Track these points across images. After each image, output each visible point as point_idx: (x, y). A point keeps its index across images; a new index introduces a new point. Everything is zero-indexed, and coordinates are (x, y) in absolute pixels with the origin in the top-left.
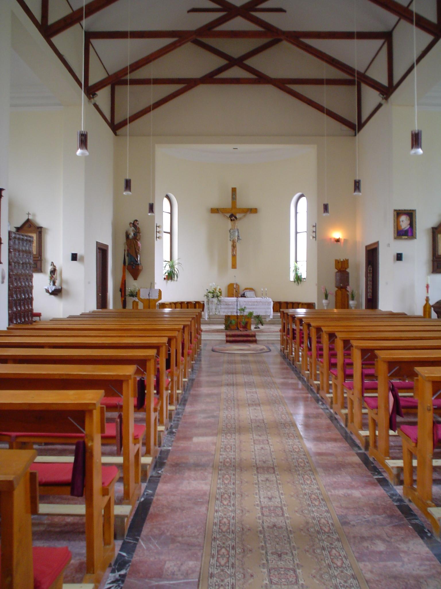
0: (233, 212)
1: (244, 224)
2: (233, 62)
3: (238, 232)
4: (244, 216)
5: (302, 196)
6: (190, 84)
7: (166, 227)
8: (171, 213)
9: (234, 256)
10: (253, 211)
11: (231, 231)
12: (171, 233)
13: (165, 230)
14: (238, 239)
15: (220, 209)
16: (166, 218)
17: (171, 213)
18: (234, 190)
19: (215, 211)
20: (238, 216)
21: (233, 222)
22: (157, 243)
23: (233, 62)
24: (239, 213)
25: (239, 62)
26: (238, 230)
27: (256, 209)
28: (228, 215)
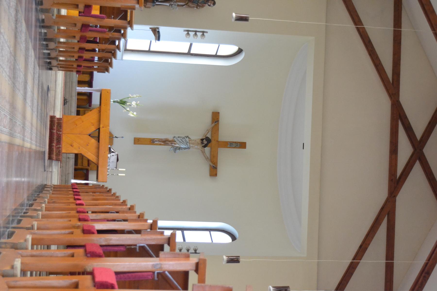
0: (213, 142)
1: (197, 160)
2: (418, 145)
3: (185, 148)
4: (207, 158)
5: (234, 238)
6: (392, 86)
7: (198, 48)
8: (216, 56)
9: (152, 142)
10: (214, 171)
11: (187, 139)
12: (189, 54)
13: (194, 44)
14: (176, 149)
15: (218, 124)
16: (209, 48)
17: (216, 56)
18: (243, 145)
19: (216, 117)
20: (207, 149)
21: (199, 142)
22: (180, 31)
23: (418, 145)
24: (211, 152)
25: (418, 155)
26: (189, 148)
27: (216, 175)
28: (209, 136)
